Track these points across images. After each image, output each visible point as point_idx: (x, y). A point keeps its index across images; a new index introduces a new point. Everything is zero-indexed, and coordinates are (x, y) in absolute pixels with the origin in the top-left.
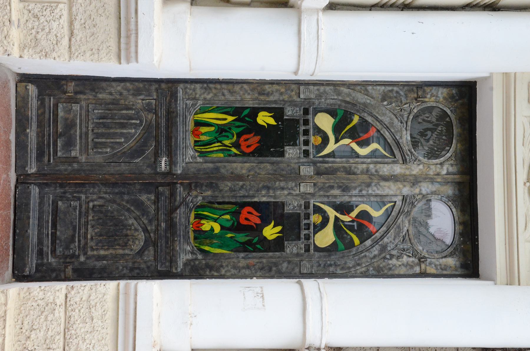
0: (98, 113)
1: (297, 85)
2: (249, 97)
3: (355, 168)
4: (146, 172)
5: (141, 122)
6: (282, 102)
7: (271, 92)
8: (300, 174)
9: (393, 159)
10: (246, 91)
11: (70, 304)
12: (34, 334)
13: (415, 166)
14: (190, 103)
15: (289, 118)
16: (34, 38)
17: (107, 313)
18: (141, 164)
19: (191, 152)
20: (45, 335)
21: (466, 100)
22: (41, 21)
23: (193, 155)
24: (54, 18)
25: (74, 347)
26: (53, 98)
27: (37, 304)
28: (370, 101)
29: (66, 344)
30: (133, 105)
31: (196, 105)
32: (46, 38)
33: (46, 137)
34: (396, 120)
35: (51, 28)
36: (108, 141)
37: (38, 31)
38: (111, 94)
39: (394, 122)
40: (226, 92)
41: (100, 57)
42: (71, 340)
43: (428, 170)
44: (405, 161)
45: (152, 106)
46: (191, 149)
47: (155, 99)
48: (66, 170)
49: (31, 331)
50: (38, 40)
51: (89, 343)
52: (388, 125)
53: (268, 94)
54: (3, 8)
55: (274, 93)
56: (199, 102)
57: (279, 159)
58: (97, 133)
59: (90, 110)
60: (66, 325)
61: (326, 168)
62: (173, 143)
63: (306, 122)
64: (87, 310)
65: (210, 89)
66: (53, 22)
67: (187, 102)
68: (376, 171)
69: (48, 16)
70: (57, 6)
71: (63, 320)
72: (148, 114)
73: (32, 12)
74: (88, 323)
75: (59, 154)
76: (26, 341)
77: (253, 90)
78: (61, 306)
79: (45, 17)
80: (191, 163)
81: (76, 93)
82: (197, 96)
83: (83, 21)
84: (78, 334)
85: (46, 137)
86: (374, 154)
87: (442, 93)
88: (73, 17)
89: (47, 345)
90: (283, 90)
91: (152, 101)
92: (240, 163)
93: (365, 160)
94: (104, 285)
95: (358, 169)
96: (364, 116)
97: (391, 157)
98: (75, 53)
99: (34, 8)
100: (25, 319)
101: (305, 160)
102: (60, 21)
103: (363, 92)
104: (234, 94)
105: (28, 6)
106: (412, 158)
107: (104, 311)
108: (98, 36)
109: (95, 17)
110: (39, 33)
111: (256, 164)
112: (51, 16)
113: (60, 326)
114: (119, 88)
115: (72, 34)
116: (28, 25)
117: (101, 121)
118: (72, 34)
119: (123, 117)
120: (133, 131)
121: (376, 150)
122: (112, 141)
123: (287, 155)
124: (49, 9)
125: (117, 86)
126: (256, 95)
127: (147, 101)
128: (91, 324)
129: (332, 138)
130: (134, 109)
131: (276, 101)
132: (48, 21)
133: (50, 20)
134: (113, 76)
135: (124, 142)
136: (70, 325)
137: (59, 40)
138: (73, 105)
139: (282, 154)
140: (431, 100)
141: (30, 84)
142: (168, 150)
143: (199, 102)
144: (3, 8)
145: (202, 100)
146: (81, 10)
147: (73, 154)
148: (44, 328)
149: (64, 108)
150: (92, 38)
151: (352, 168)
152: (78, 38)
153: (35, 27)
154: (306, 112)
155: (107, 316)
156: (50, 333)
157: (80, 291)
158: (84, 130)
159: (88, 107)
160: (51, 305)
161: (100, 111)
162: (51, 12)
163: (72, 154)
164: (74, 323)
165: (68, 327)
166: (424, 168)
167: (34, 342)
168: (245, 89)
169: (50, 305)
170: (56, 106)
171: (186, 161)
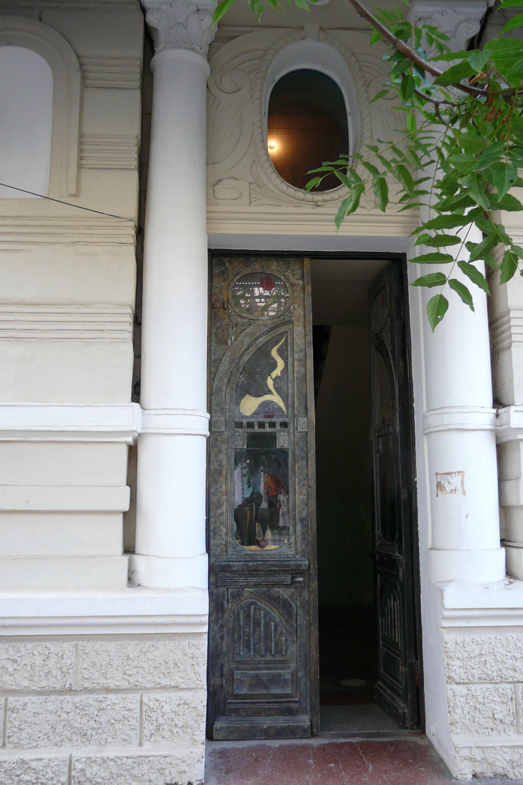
0: (243, 651)
6: (229, 450)
9: (288, 334)
10: (217, 489)
11: (466, 680)
12: (498, 715)
13: (295, 312)
16: (182, 729)
17: (475, 640)
18: (298, 603)
20: (498, 703)
21: (226, 260)
22: (163, 722)
24: (159, 708)
25: (510, 672)
26: (228, 700)
28: (227, 357)
29: (507, 681)
30: (234, 612)
32: (182, 717)
33: (272, 706)
34: (247, 331)
35: (171, 711)
36: (273, 639)
37: (174, 725)
38: (222, 637)
39: (250, 332)
41: (201, 655)
42: (503, 676)
44: (290, 322)
45: (235, 592)
46: (281, 549)
47: (228, 589)
48: (305, 684)
49: (495, 719)
50: (184, 725)
51: (506, 656)
52: (253, 339)
53: (221, 466)
54: (151, 764)
57: (290, 454)
58: (266, 651)
59: (240, 660)
60: (487, 681)
61: (299, 404)
63: (250, 425)
64: (472, 661)
65: (215, 528)
66: (163, 709)
68: (301, 351)
69: (158, 714)
70: (145, 704)
71: (483, 686)
72: (244, 596)
73: (153, 732)
74: (486, 659)
75: (289, 691)
76: (504, 723)
77: (216, 482)
78: (470, 688)
79: (158, 718)
81: (222, 675)
82: (224, 543)
83: (162, 676)
84: (497, 669)
85: (272, 706)
86: (281, 352)
87: (218, 283)
88: (157, 686)
89: (508, 701)
90: (216, 450)
91: (229, 592)
92: (295, 495)
94: (446, 643)
95: (299, 370)
96: (243, 363)
97: (285, 336)
98: (197, 684)
99: (149, 730)
100: (483, 725)
101: (291, 426)
102: (162, 700)
103: (217, 365)
105: (146, 736)
107: (473, 642)
108: (178, 659)
109: (157, 662)
110: (176, 724)
112: (157, 711)
113: (489, 688)
115: (176, 688)
116: (168, 737)
117: (252, 648)
118: (176, 688)
119: (247, 624)
120: (262, 612)
122: (273, 634)
123: (286, 446)
124: (150, 714)
127: (229, 597)
128: (486, 655)
131: (228, 457)
132: (163, 714)
133: (162, 712)
136: (488, 678)
137: (183, 702)
138: (235, 678)
139: (284, 452)
140: (226, 294)
141: (214, 726)
142: (283, 574)
144: (151, 764)
146: (149, 677)
147: (288, 676)
148: (492, 705)
150: (180, 665)
151: (299, 376)
152: (181, 680)
153: (170, 728)
154: (239, 425)
155: (478, 639)
156: (497, 699)
157: (453, 669)
158: (263, 666)
159: (236, 661)
160: (468, 699)
161: (241, 649)
162: (152, 711)
164: (486, 674)
165: (489, 679)
166: (297, 303)
167: (506, 715)
168: (215, 491)
169: (468, 701)
170: (236, 696)
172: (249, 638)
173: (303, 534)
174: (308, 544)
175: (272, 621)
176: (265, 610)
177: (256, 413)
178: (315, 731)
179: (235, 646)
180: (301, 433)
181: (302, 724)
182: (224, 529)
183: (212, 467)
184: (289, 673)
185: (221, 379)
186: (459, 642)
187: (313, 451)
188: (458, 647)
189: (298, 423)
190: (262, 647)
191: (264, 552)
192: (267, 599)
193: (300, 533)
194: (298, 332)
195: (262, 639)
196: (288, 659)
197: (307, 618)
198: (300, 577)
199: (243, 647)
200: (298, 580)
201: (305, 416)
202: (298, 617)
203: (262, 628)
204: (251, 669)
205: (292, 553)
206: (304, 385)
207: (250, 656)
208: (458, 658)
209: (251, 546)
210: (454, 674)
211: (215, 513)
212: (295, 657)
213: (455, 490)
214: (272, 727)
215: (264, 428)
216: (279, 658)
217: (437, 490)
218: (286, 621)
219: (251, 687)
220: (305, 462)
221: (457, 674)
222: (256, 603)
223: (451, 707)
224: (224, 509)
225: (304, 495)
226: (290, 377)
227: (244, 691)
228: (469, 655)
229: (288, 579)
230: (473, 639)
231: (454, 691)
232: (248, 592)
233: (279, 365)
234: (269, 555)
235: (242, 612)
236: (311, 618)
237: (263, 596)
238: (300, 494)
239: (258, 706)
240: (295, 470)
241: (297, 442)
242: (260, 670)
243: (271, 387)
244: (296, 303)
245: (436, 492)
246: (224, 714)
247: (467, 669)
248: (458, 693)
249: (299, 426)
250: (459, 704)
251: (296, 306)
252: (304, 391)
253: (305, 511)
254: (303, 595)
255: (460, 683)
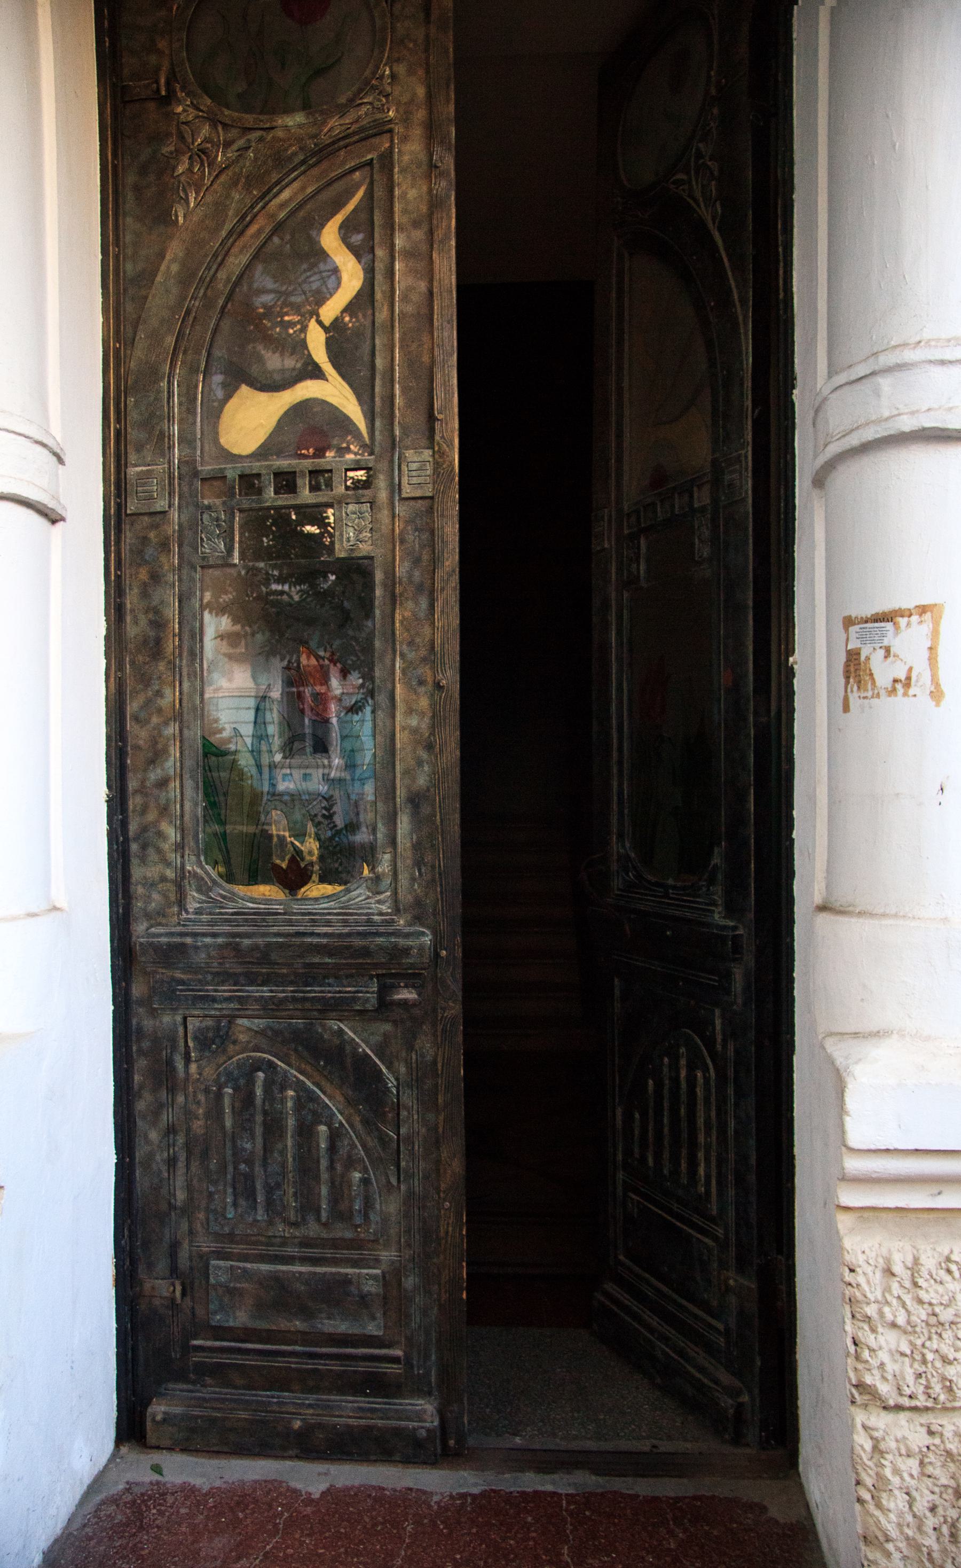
1: (126, 527)
2: (168, 691)
3: (405, 298)
4: (432, 1052)
5: (257, 1066)
7: (151, 616)
8: (432, 498)
10: (148, 702)
11: (922, 1397)
14: (193, 897)
15: (237, 545)
18: (403, 1069)
19: (359, 894)
23: (369, 889)
26: (195, 1339)
27: (928, 1514)
30: (207, 1091)
31: (203, 879)
36: (325, 1176)
38: (172, 1162)
40: (154, 775)
43: (411, 45)
45: (208, 1028)
46: (348, 896)
47: (185, 1019)
48: (425, 1312)
55: (154, 603)
56: (189, 868)
57: (379, 576)
59: (227, 1230)
62: (327, 960)
63: (249, 482)
65: (144, 829)
67: (191, 910)
68: (416, 224)
72: (235, 1042)
75: (372, 1329)
77: (145, 680)
80: (395, 893)
82: (170, 874)
91: (190, 1027)
92: (393, 717)
93: (380, 266)
95: (410, 289)
96: (228, 280)
104: (160, 746)
106: (370, 103)
107: (949, 1271)
111: (398, 659)
114: (154, 1135)
120: (291, 1093)
121: (346, 230)
122: (324, 1163)
123: (365, 549)
125: (147, 1141)
126: (162, 666)
127: (191, 1044)
129: (308, 390)
130: (220, 1088)
134: (111, 1158)
135: (330, 1127)
138: (212, 1281)
142: (352, 976)
143: (189, 868)
145: (183, 857)
149: (222, 1308)
163: (373, 1290)
168: (142, 708)
170: (219, 1332)
171: (390, 914)
172: (252, 1170)
173: (417, 847)
174: (433, 880)
175: (321, 1123)
176: (300, 1086)
177: (263, 452)
178: (452, 1443)
179: (212, 1189)
180: (412, 503)
181: (411, 1425)
182: (172, 833)
183: (132, 630)
184: (374, 1277)
185: (156, 338)
186: (898, 1268)
187: (451, 559)
188: (895, 1286)
189: (404, 468)
190: (291, 1200)
191: (296, 907)
192: (305, 1054)
193: (409, 845)
194: (406, 158)
195: (291, 1175)
196: (372, 1238)
197: (431, 1116)
198: (406, 986)
199: (235, 1195)
200: (400, 997)
201: (424, 442)
202: (404, 1113)
203: (290, 1142)
204: (262, 1258)
205: (384, 908)
206: (425, 338)
207: (256, 1221)
208: (894, 1325)
209: (256, 887)
210: (878, 1377)
211: (143, 781)
212: (393, 1232)
213: (908, 683)
214: (320, 1426)
215: (296, 493)
216: (342, 1232)
217: (847, 683)
218: (366, 1122)
219: (260, 1308)
220: (424, 603)
221: (890, 1377)
222: (271, 1065)
223: (865, 1486)
224: (171, 764)
225: (423, 714)
226: (382, 315)
227: (241, 1318)
228: (935, 1315)
229: (369, 993)
230: (948, 1259)
231: (876, 1434)
232: (250, 1029)
233: (345, 277)
234: (310, 914)
235: (230, 1091)
236: (441, 1118)
237: (293, 1046)
238: (410, 711)
239: (280, 1363)
240: (393, 634)
241: (401, 533)
242: (287, 1264)
243: (320, 354)
244: (398, 60)
245: (842, 693)
246: (181, 1376)
247: (924, 1361)
248: (893, 1445)
249: (405, 480)
250: (896, 1481)
251: (401, 69)
252: (426, 359)
253: (426, 768)
254: (418, 1044)
255: (899, 1408)
